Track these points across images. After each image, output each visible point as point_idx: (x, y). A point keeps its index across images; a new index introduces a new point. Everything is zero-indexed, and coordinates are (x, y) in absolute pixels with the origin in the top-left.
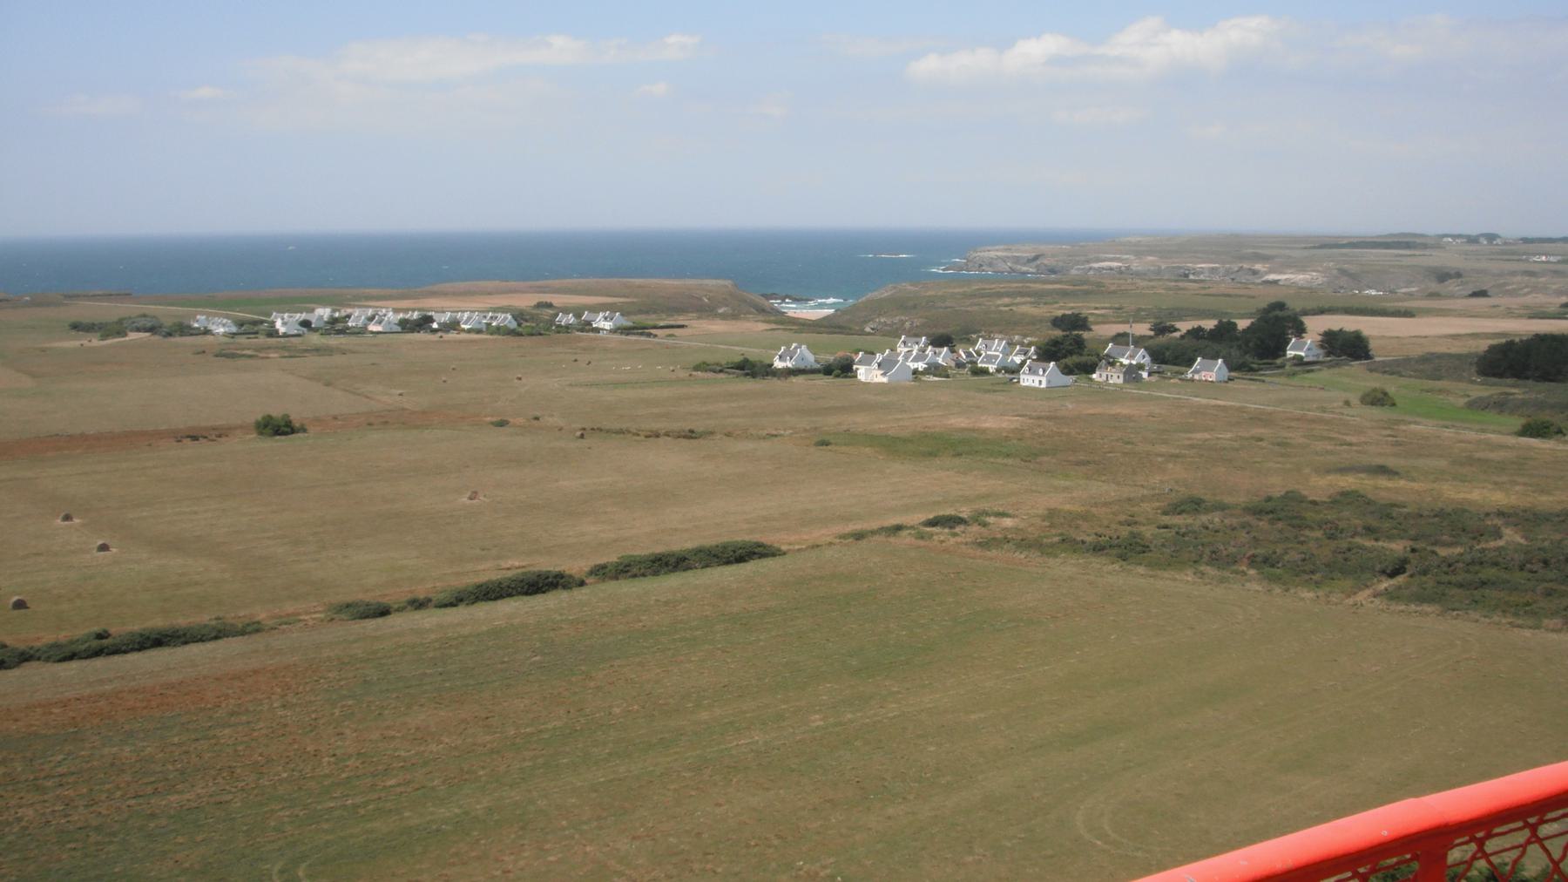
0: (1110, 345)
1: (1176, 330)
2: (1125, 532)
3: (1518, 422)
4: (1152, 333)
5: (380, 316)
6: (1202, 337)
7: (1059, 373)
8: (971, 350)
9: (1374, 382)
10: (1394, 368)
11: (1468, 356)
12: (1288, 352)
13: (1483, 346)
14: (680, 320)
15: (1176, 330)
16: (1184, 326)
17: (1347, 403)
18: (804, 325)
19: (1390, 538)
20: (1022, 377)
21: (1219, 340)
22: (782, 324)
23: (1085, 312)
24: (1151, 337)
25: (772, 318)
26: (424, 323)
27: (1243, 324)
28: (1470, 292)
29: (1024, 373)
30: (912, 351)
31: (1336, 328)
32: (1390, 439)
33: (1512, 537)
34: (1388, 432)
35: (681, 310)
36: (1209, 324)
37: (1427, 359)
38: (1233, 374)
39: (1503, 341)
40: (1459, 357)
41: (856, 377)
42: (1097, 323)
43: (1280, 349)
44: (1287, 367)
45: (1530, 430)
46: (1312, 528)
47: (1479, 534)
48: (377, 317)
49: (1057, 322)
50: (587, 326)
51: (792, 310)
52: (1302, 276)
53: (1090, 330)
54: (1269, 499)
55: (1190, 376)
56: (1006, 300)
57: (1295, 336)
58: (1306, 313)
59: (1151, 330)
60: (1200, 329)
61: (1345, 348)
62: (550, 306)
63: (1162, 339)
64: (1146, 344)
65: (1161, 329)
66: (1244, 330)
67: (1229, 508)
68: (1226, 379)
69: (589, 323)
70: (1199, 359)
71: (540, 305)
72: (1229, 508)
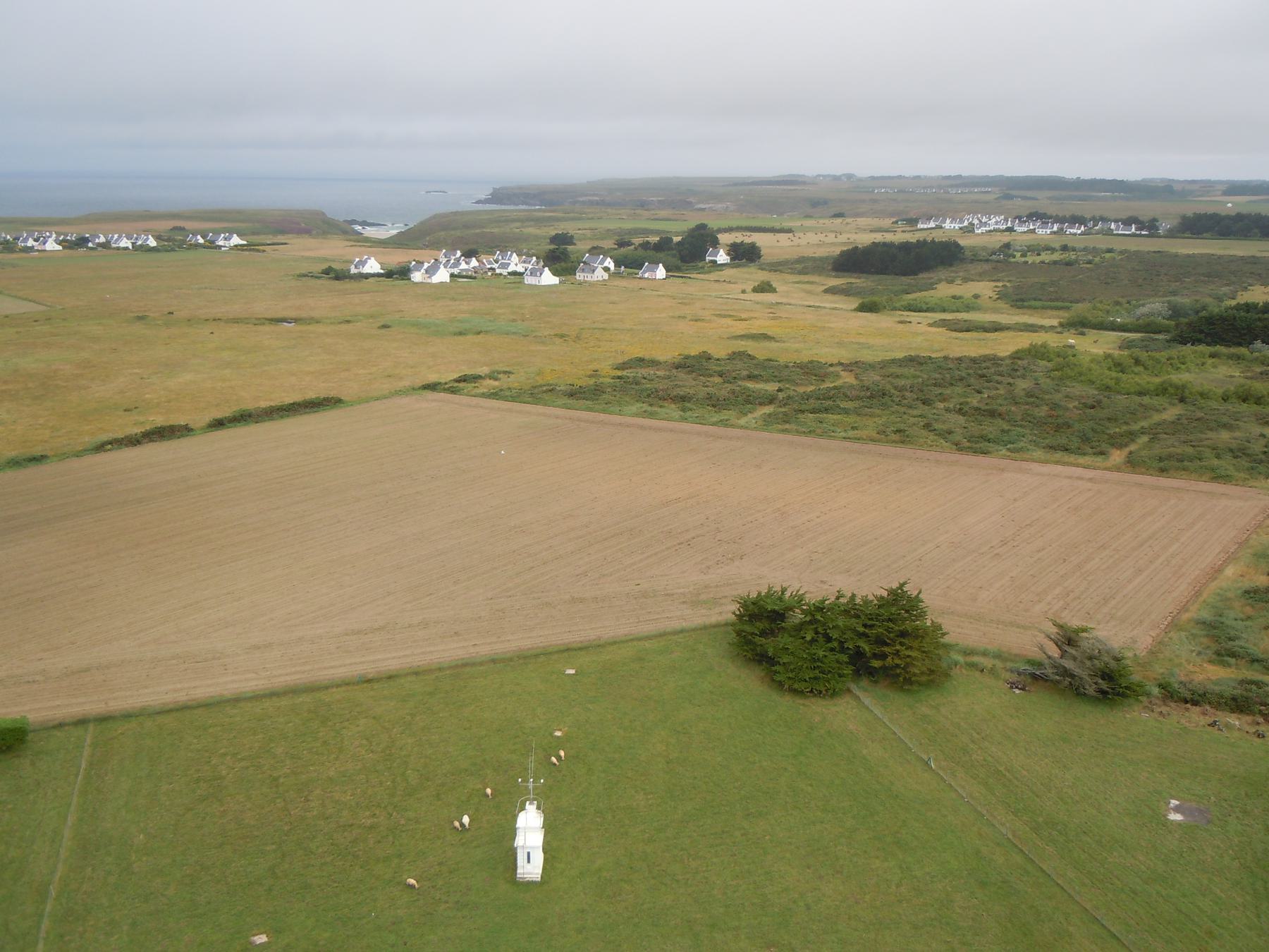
0: (587, 255)
1: (632, 244)
2: (592, 382)
3: (855, 303)
4: (616, 246)
5: (44, 237)
6: (649, 249)
7: (551, 275)
8: (492, 259)
9: (762, 276)
10: (777, 267)
11: (827, 258)
12: (707, 258)
13: (837, 251)
14: (280, 239)
15: (632, 244)
16: (637, 241)
17: (744, 292)
18: (374, 242)
19: (767, 381)
20: (526, 277)
21: (660, 249)
22: (359, 242)
23: (571, 232)
24: (615, 249)
25: (352, 237)
26: (82, 242)
27: (677, 239)
28: (833, 214)
29: (527, 275)
30: (450, 260)
31: (738, 241)
32: (771, 315)
33: (848, 379)
34: (770, 311)
35: (283, 232)
36: (654, 239)
37: (801, 260)
38: (669, 274)
39: (851, 247)
40: (821, 259)
41: (410, 279)
42: (580, 240)
43: (700, 255)
44: (706, 268)
45: (863, 308)
46: (1236, 549)
47: (822, 378)
48: (42, 239)
49: (554, 239)
50: (211, 245)
51: (370, 232)
52: (720, 206)
53: (575, 244)
54: (687, 357)
55: (640, 275)
56: (518, 224)
57: (712, 247)
58: (720, 231)
59: (615, 244)
60: (648, 242)
61: (744, 254)
62: (182, 229)
63: (623, 250)
64: (612, 254)
65: (621, 244)
66: (523, 808)
67: (779, 431)
68: (664, 277)
69: (212, 242)
70: (646, 264)
71: (175, 229)
72: (779, 431)
